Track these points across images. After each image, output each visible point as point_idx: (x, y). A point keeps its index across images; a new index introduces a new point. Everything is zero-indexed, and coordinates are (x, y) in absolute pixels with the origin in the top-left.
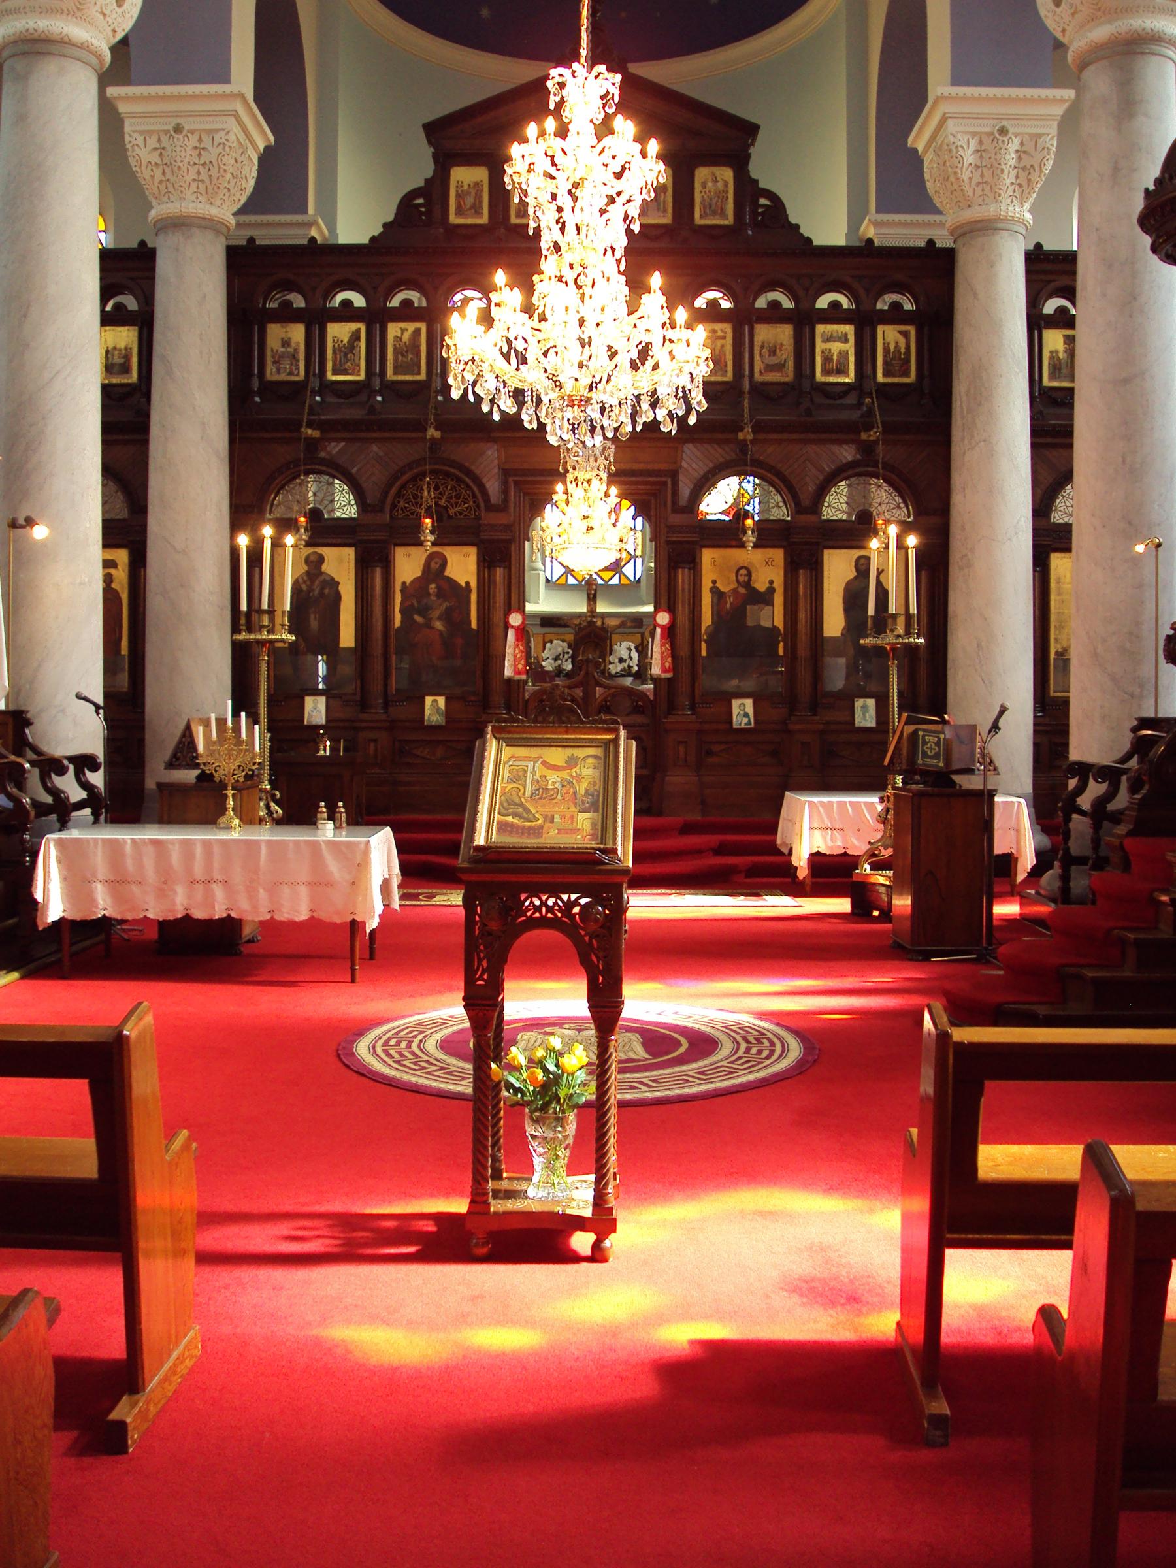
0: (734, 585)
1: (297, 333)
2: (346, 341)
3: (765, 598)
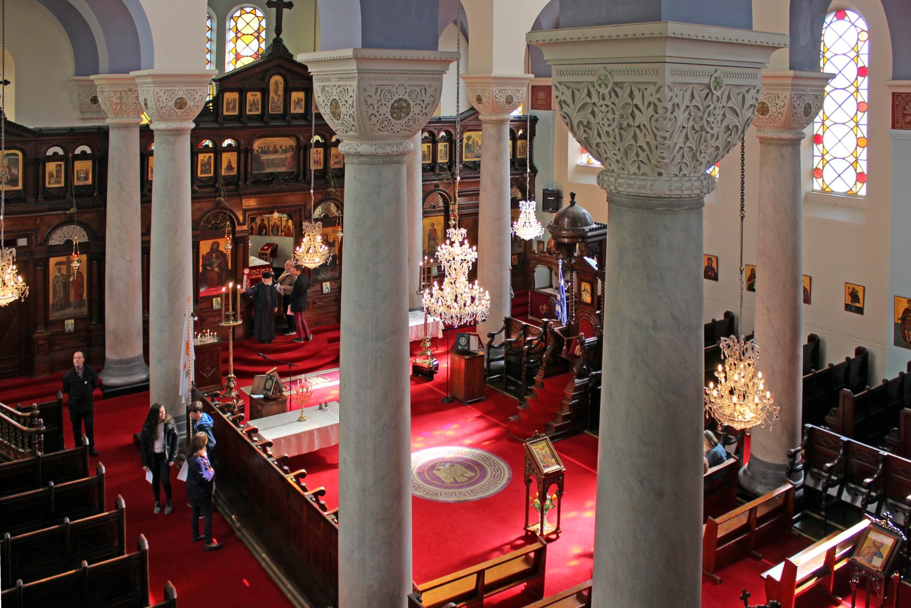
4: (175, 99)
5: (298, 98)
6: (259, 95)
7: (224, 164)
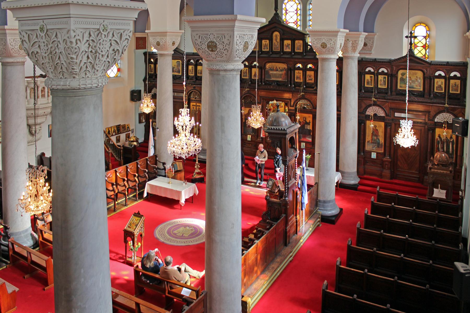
0: (303, 121)
3: (308, 124)
6: (268, 41)
7: (253, 74)
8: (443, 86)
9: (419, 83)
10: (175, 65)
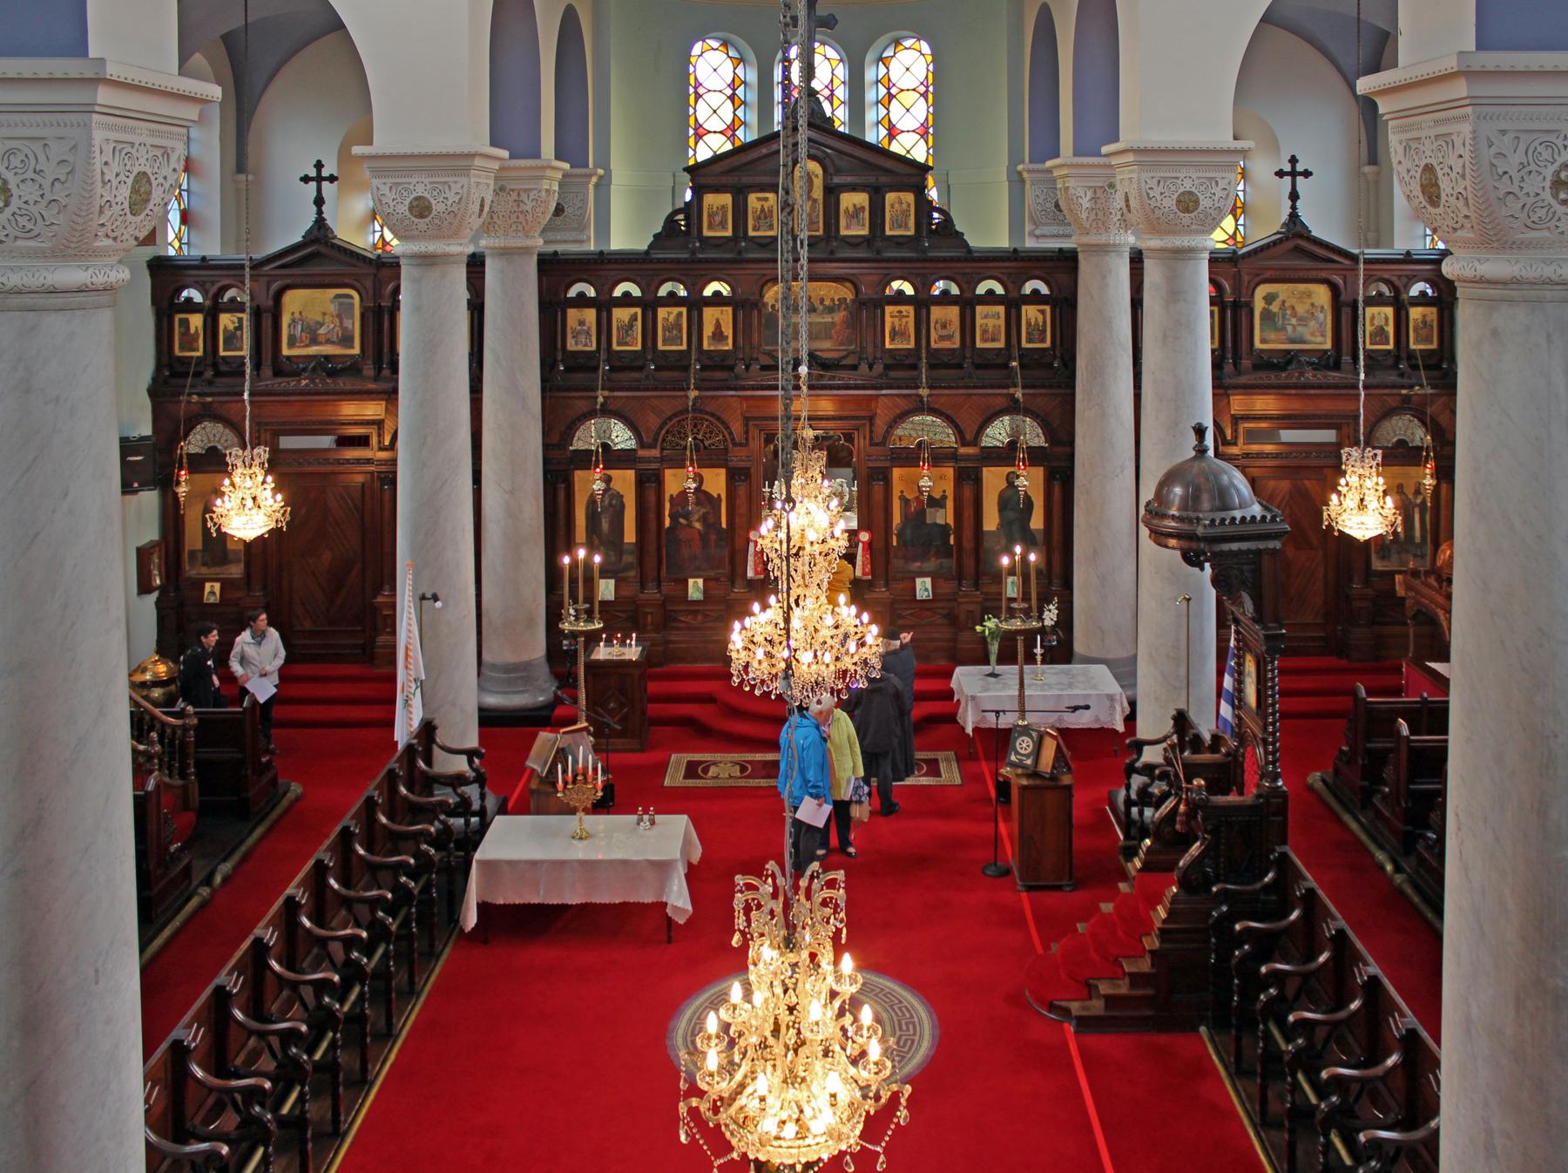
1: (590, 315)
2: (626, 322)
4: (409, 200)
5: (855, 205)
7: (708, 330)
8: (1390, 329)
9: (1321, 324)
10: (324, 314)
